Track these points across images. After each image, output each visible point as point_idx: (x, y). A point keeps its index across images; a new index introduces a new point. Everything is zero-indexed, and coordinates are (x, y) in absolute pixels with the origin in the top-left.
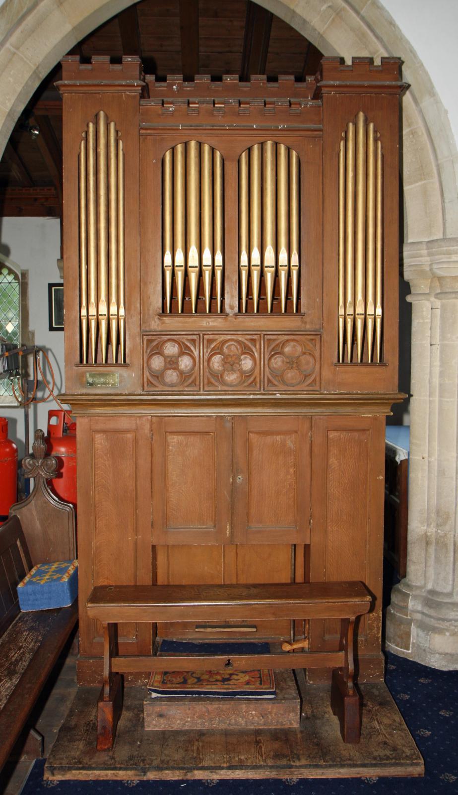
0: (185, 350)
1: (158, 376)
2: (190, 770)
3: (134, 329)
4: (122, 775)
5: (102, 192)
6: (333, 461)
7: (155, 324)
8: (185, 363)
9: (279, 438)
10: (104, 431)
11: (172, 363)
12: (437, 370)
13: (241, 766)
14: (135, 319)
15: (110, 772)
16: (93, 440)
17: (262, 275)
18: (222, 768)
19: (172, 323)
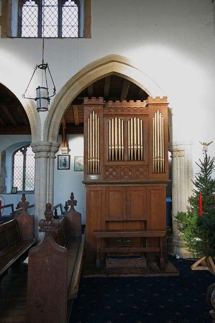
0: (114, 170)
1: (107, 177)
2: (119, 274)
3: (102, 164)
4: (103, 276)
5: (94, 138)
6: (152, 198)
7: (107, 164)
8: (114, 173)
9: (138, 192)
10: (94, 191)
11: (111, 173)
12: (179, 176)
13: (132, 273)
14: (102, 162)
15: (99, 275)
16: (90, 193)
17: (160, 162)
18: (128, 274)
19: (111, 163)
